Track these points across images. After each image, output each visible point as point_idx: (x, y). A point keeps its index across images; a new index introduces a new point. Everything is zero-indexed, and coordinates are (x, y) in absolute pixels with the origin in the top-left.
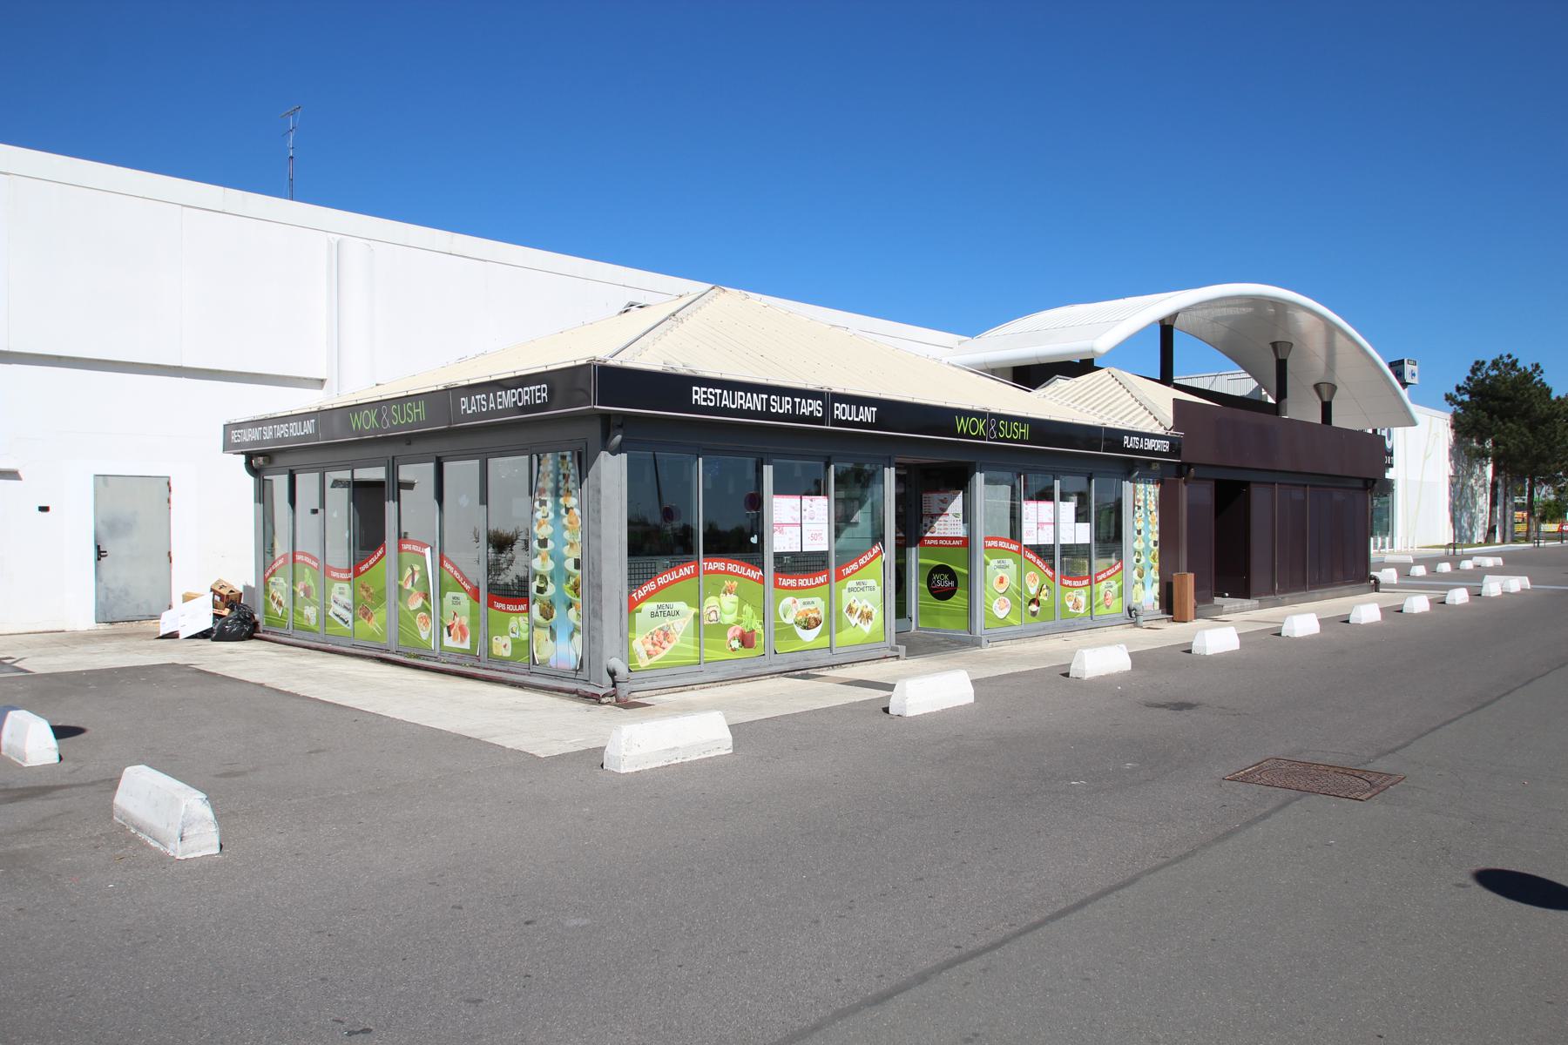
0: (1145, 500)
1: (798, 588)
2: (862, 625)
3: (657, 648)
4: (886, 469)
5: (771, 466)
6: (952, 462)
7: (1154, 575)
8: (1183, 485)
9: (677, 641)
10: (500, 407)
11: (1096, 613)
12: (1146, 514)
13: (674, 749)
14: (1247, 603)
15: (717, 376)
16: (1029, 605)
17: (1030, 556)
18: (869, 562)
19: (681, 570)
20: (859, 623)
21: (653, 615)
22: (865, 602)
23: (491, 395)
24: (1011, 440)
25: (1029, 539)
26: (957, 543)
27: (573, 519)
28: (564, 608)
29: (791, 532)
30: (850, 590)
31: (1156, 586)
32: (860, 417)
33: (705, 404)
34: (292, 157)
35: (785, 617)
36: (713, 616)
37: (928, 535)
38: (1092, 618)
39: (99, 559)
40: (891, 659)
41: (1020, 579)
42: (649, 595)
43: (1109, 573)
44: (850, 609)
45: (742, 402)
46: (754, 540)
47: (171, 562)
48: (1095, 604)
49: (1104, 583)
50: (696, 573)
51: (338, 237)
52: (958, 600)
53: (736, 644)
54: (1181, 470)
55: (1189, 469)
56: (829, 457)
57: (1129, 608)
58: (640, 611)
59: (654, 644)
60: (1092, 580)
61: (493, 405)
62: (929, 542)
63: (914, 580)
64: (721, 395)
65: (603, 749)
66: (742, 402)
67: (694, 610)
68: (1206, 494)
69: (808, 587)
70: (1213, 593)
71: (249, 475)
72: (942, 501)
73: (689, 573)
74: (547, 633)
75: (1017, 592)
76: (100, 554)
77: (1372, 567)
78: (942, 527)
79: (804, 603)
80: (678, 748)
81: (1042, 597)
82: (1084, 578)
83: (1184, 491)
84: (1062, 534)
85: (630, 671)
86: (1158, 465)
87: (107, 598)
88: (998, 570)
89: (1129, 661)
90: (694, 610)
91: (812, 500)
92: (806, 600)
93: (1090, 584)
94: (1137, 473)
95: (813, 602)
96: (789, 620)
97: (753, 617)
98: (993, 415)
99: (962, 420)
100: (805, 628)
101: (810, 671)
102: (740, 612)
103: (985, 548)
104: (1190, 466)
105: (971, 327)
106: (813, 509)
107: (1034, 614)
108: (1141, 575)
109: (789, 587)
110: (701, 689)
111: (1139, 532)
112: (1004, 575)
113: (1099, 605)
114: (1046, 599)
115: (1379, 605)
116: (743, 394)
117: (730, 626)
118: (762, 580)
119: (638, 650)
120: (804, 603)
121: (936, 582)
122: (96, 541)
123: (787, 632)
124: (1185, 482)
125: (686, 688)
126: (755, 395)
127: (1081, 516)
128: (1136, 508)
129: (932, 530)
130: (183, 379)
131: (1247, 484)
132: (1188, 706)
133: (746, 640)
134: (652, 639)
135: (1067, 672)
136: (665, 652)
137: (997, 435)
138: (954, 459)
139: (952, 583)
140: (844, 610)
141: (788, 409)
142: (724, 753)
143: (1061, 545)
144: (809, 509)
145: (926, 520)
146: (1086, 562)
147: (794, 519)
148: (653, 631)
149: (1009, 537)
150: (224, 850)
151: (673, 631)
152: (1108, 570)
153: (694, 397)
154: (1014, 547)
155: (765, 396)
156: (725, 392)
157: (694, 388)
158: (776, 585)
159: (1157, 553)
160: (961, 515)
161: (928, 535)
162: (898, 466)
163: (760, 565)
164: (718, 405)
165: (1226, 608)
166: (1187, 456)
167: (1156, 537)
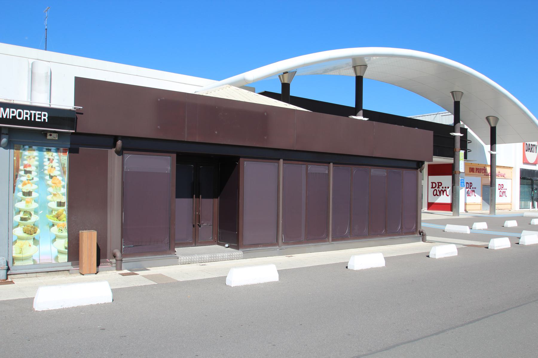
12: (42, 178)
65: (348, 262)
74: (31, 242)
77: (422, 221)
89: (456, 251)
104: (116, 138)
115: (277, 267)
135: (518, 242)
150: (114, 301)
164: (33, 120)
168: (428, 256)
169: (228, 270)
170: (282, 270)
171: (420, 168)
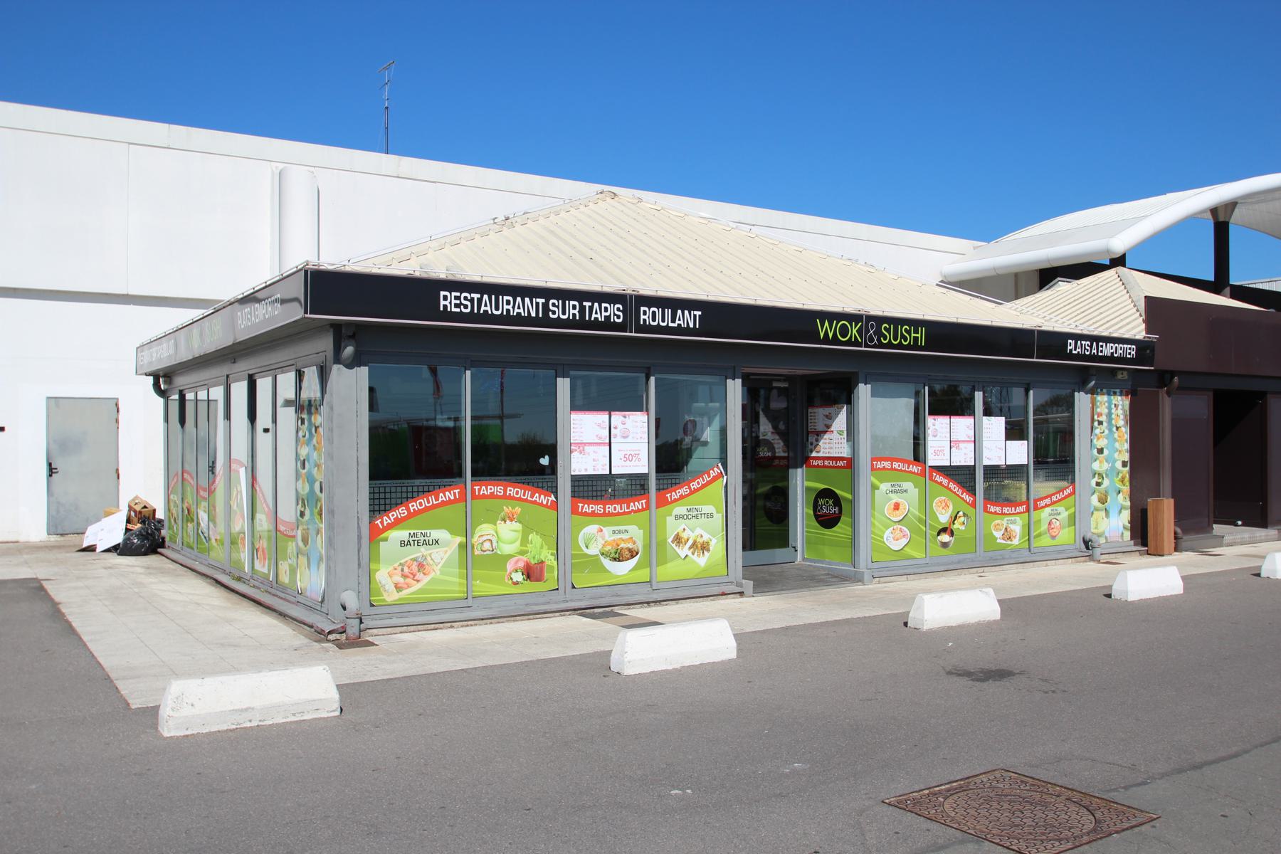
0: (1109, 415)
1: (605, 514)
2: (695, 557)
3: (408, 580)
4: (729, 382)
5: (569, 379)
6: (835, 373)
7: (1124, 500)
8: (1165, 395)
9: (436, 572)
10: (1100, 354)
11: (1035, 544)
12: (1110, 430)
13: (247, 709)
14: (1260, 532)
15: (477, 279)
16: (938, 535)
17: (939, 478)
18: (704, 486)
19: (537, 495)
20: (690, 554)
21: (403, 544)
22: (698, 531)
23: (1095, 343)
24: (900, 346)
25: (933, 460)
26: (841, 463)
27: (1121, 434)
28: (1115, 494)
29: (966, 448)
30: (678, 517)
31: (1126, 515)
32: (677, 322)
33: (458, 310)
34: (387, 108)
35: (587, 547)
36: (487, 546)
37: (814, 454)
38: (1030, 551)
39: (51, 476)
40: (732, 596)
41: (925, 503)
42: (397, 523)
43: (1054, 498)
44: (678, 539)
45: (510, 307)
46: (545, 461)
47: (118, 478)
48: (1034, 534)
49: (1048, 510)
50: (463, 498)
51: (281, 166)
52: (841, 529)
53: (518, 577)
54: (1163, 378)
55: (1172, 378)
56: (649, 368)
57: (1084, 539)
58: (386, 540)
59: (405, 576)
60: (1031, 506)
61: (1095, 351)
62: (815, 463)
63: (799, 504)
64: (480, 300)
66: (510, 307)
67: (460, 539)
68: (1200, 407)
69: (619, 514)
70: (1212, 519)
71: (158, 397)
72: (827, 416)
73: (452, 498)
74: (1103, 513)
75: (920, 520)
76: (51, 470)
78: (827, 446)
79: (614, 532)
80: (253, 709)
81: (956, 526)
82: (1021, 504)
83: (1166, 406)
84: (986, 453)
85: (372, 605)
86: (1125, 373)
87: (58, 512)
88: (891, 495)
89: (997, 608)
90: (460, 539)
91: (625, 417)
92: (615, 528)
93: (1028, 510)
94: (1093, 382)
95: (627, 531)
96: (594, 550)
97: (542, 547)
98: (870, 318)
99: (827, 324)
100: (615, 559)
101: (616, 610)
102: (525, 541)
103: (873, 469)
104: (1173, 374)
105: (987, 231)
106: (936, 427)
107: (945, 545)
108: (1103, 501)
109: (593, 514)
110: (462, 626)
111: (1100, 451)
112: (900, 500)
113: (1039, 535)
114: (963, 528)
116: (510, 298)
117: (510, 556)
118: (555, 506)
119: (383, 582)
120: (614, 532)
121: (821, 508)
122: (48, 459)
123: (593, 564)
124: (1168, 393)
125: (441, 625)
126: (527, 300)
127: (1015, 432)
128: (1096, 424)
129: (817, 449)
130: (131, 307)
131: (1262, 395)
132: (1001, 674)
133: (532, 572)
134: (402, 570)
135: (1109, 593)
136: (419, 586)
137: (879, 340)
138: (836, 370)
139: (837, 509)
140: (670, 540)
141: (574, 315)
142: (325, 715)
143: (985, 467)
144: (620, 427)
145: (812, 438)
146: (1024, 485)
147: (600, 438)
148: (402, 561)
149: (911, 458)
151: (431, 562)
152: (1054, 494)
153: (442, 302)
154: (916, 469)
155: (541, 301)
156: (486, 297)
157: (442, 293)
158: (575, 511)
159: (1128, 476)
160: (845, 432)
161: (814, 454)
162: (746, 380)
163: (554, 490)
164: (476, 311)
165: (1228, 539)
166: (1163, 361)
167: (1126, 457)
168: (1109, 596)
169: (911, 600)
170: (1001, 600)
171: (1165, 386)
